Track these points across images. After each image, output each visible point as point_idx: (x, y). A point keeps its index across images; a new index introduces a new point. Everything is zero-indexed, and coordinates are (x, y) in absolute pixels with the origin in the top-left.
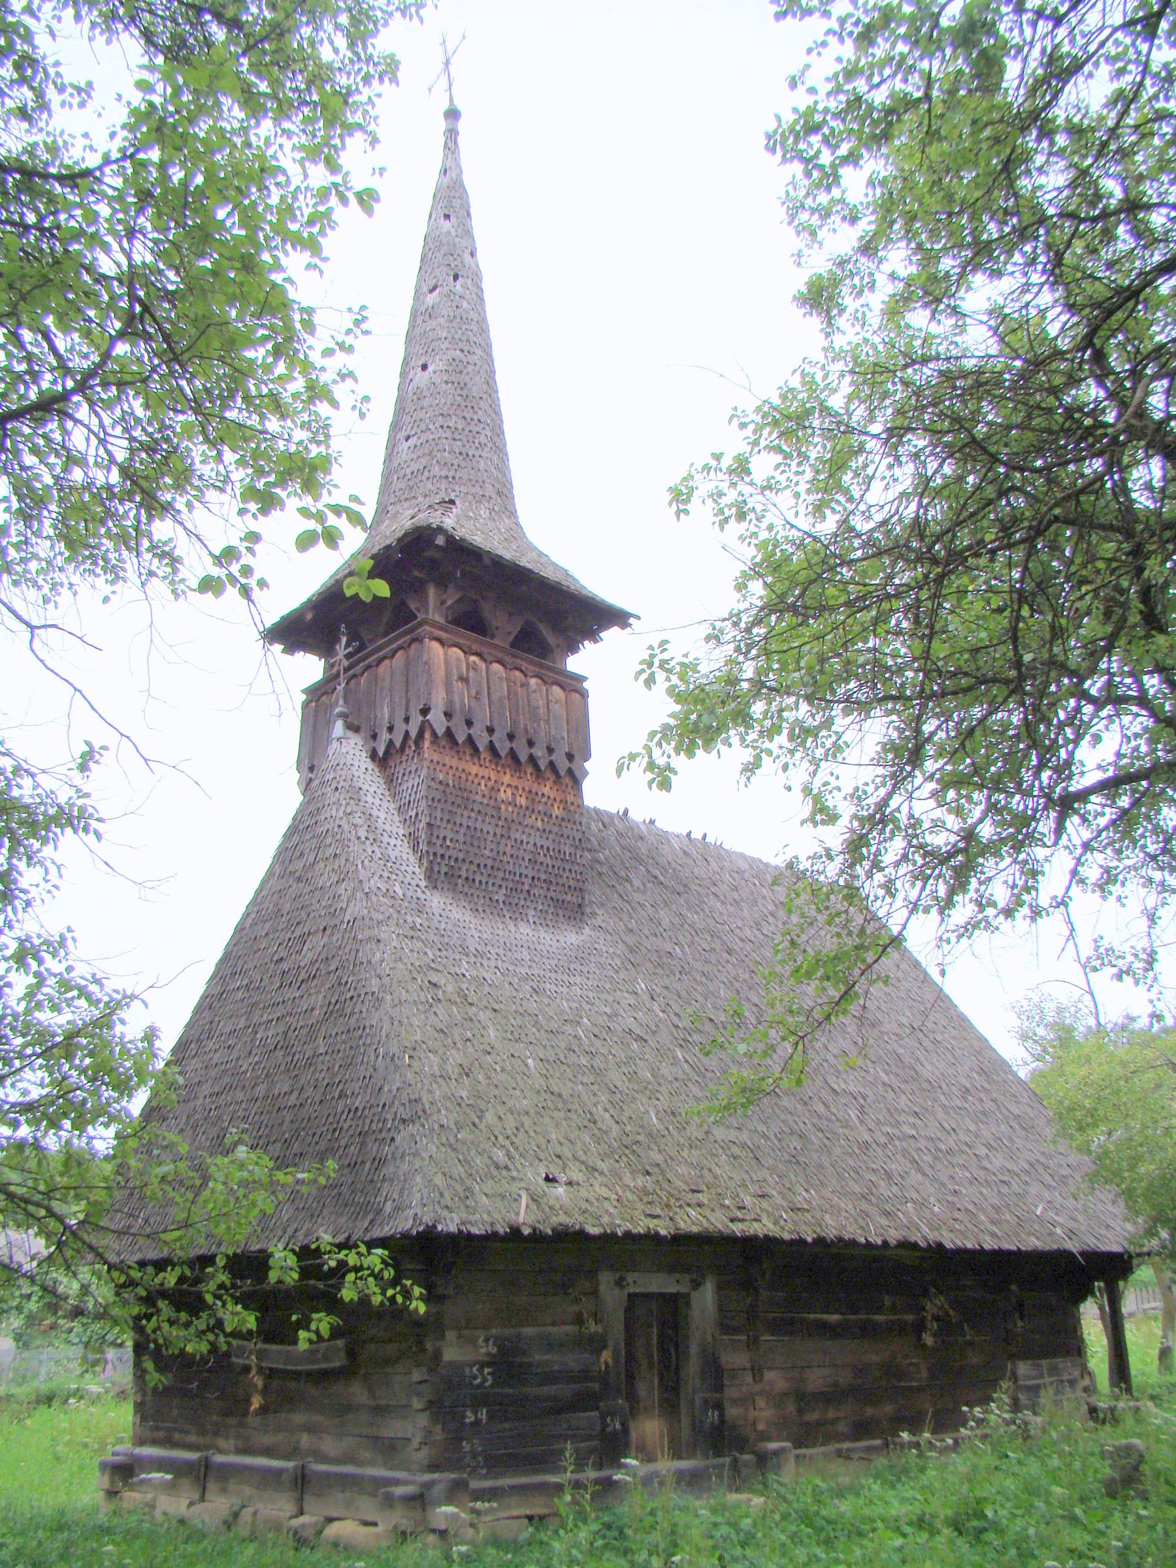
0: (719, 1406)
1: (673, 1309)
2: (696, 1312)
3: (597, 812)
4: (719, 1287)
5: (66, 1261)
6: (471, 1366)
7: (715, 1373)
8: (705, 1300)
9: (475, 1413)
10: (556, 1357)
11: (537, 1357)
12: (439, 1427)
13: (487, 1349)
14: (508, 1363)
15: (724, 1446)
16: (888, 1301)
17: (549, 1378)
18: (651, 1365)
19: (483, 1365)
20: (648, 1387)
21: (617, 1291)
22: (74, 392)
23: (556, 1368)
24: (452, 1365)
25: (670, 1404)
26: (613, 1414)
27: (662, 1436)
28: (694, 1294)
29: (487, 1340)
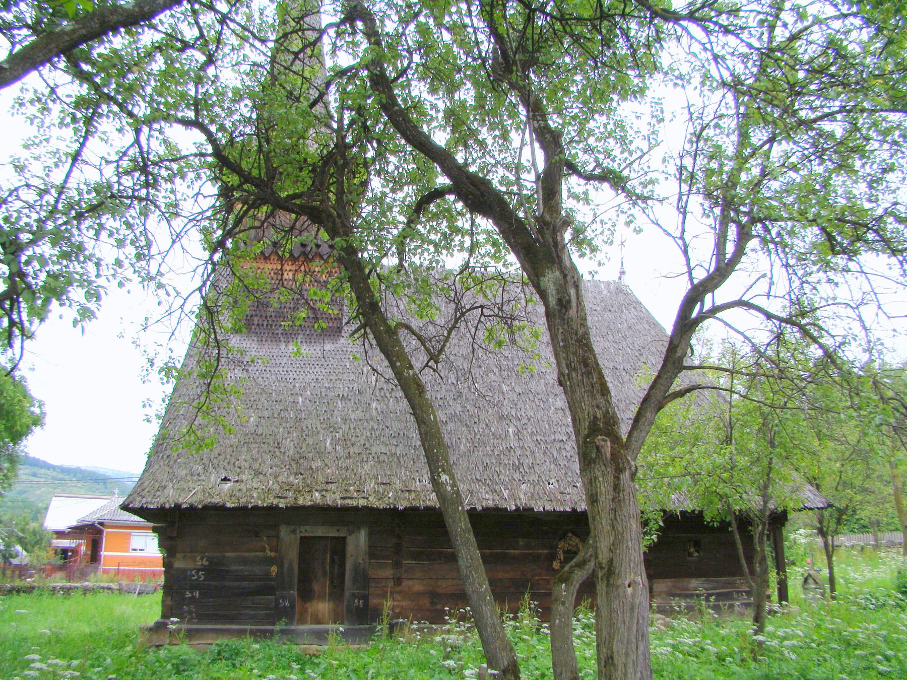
0: (366, 598)
1: (339, 547)
2: (350, 548)
3: (161, 449)
4: (370, 534)
5: (60, 194)
6: (191, 571)
7: (363, 579)
8: (359, 542)
9: (192, 593)
10: (247, 568)
11: (235, 568)
12: (169, 598)
13: (200, 562)
14: (215, 570)
15: (362, 618)
16: (521, 542)
17: (242, 578)
18: (324, 573)
19: (198, 570)
20: (321, 584)
21: (293, 536)
22: (47, 219)
23: (246, 573)
24: (178, 569)
25: (337, 591)
26: (284, 598)
27: (712, 581)
28: (349, 537)
29: (202, 559)
